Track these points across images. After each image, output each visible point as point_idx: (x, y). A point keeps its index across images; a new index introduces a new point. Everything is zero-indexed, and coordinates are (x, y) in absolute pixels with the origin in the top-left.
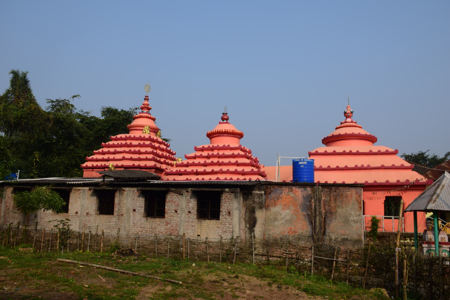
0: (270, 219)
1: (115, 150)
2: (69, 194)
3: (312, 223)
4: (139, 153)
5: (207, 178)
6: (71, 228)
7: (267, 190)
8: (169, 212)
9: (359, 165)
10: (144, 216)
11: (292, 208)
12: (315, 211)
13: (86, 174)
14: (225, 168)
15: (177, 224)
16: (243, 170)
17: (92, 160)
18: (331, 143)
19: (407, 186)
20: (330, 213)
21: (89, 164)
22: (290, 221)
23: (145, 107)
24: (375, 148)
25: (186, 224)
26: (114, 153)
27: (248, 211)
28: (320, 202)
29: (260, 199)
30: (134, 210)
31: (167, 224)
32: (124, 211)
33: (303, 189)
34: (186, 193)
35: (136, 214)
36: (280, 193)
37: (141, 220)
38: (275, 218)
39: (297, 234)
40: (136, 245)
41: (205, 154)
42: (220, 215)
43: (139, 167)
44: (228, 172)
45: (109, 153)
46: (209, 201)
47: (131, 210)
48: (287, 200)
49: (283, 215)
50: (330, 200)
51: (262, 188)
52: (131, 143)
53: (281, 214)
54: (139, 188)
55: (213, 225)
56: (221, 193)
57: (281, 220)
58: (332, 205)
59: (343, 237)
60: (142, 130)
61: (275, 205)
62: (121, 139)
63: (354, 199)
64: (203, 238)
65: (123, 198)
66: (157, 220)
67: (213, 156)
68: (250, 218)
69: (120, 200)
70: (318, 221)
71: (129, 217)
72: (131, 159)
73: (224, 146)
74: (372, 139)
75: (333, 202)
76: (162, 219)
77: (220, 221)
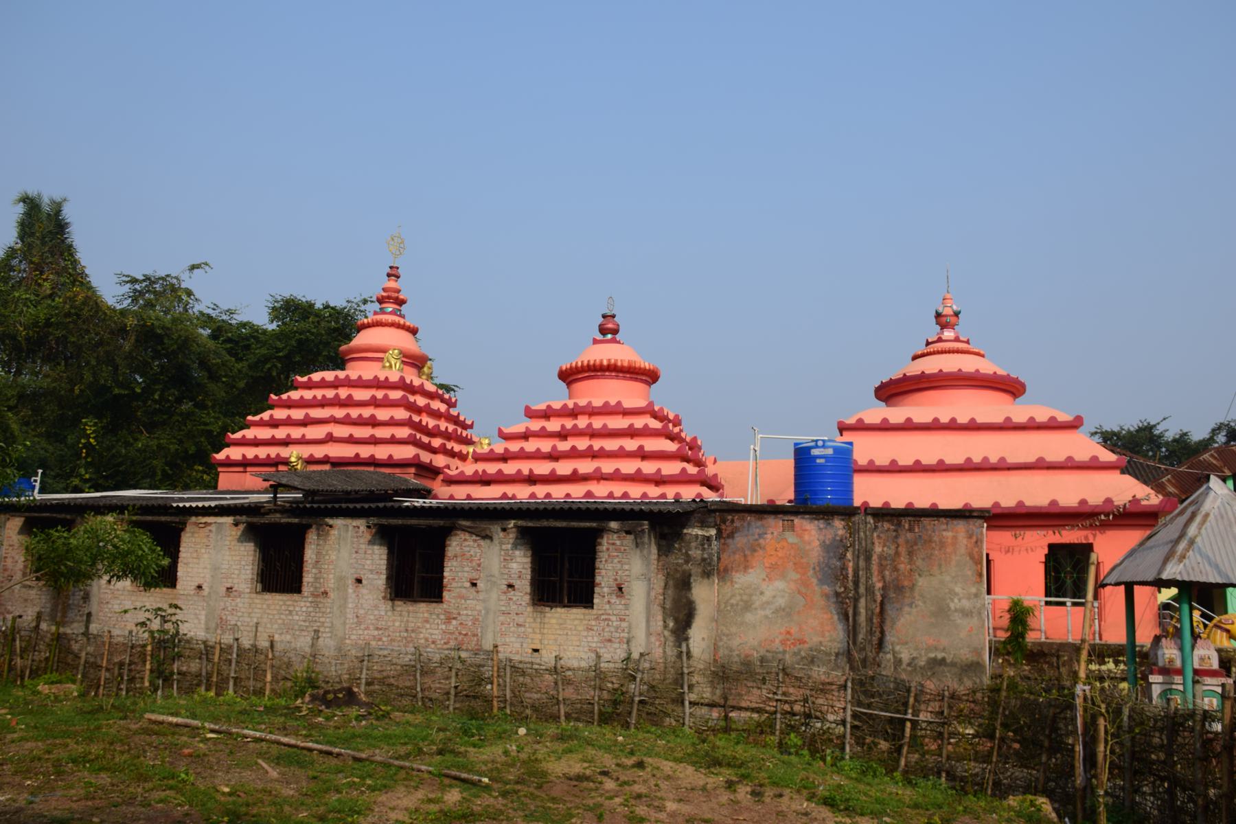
0: (732, 605)
1: (307, 414)
2: (180, 537)
3: (847, 616)
4: (373, 422)
5: (558, 493)
6: (183, 629)
7: (723, 527)
8: (454, 585)
9: (977, 459)
10: (384, 598)
11: (794, 576)
12: (856, 583)
13: (226, 480)
14: (608, 467)
15: (477, 620)
16: (659, 470)
17: (244, 443)
18: (900, 398)
19: (1107, 515)
20: (896, 591)
21: (235, 453)
22: (786, 612)
23: (389, 297)
24: (1019, 411)
25: (502, 618)
26: (305, 423)
27: (671, 583)
28: (868, 559)
29: (704, 549)
30: (359, 581)
31: (449, 619)
32: (330, 583)
33: (821, 524)
34: (502, 534)
35: (364, 591)
36: (760, 536)
37: (376, 607)
38: (746, 602)
39: (806, 646)
40: (363, 676)
41: (554, 425)
42: (596, 596)
43: (372, 462)
44: (616, 477)
45: (289, 422)
46: (563, 555)
47: (350, 581)
48: (780, 554)
49: (768, 594)
50: (897, 554)
51: (711, 520)
52: (350, 396)
53: (762, 593)
54: (374, 520)
55: (576, 622)
56: (597, 534)
57: (763, 607)
58: (902, 566)
59: (932, 655)
60: (380, 360)
61: (746, 568)
62: (323, 384)
63: (963, 550)
64: (547, 658)
65: (327, 547)
66: (422, 608)
67: (577, 433)
68: (676, 602)
69: (318, 553)
70: (863, 611)
71: (345, 599)
72: (351, 440)
73: (606, 404)
74: (1011, 388)
75: (904, 558)
76: (434, 605)
77: (594, 612)
